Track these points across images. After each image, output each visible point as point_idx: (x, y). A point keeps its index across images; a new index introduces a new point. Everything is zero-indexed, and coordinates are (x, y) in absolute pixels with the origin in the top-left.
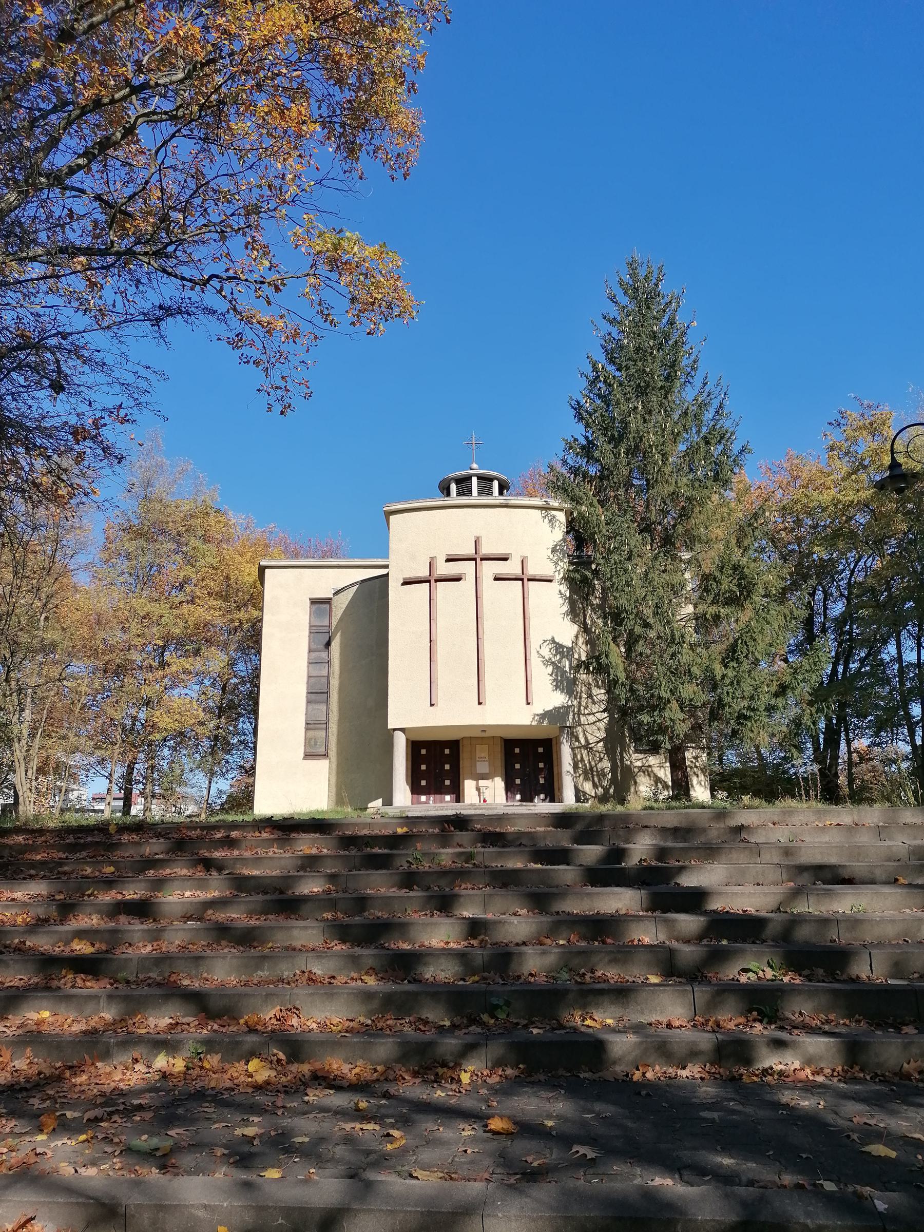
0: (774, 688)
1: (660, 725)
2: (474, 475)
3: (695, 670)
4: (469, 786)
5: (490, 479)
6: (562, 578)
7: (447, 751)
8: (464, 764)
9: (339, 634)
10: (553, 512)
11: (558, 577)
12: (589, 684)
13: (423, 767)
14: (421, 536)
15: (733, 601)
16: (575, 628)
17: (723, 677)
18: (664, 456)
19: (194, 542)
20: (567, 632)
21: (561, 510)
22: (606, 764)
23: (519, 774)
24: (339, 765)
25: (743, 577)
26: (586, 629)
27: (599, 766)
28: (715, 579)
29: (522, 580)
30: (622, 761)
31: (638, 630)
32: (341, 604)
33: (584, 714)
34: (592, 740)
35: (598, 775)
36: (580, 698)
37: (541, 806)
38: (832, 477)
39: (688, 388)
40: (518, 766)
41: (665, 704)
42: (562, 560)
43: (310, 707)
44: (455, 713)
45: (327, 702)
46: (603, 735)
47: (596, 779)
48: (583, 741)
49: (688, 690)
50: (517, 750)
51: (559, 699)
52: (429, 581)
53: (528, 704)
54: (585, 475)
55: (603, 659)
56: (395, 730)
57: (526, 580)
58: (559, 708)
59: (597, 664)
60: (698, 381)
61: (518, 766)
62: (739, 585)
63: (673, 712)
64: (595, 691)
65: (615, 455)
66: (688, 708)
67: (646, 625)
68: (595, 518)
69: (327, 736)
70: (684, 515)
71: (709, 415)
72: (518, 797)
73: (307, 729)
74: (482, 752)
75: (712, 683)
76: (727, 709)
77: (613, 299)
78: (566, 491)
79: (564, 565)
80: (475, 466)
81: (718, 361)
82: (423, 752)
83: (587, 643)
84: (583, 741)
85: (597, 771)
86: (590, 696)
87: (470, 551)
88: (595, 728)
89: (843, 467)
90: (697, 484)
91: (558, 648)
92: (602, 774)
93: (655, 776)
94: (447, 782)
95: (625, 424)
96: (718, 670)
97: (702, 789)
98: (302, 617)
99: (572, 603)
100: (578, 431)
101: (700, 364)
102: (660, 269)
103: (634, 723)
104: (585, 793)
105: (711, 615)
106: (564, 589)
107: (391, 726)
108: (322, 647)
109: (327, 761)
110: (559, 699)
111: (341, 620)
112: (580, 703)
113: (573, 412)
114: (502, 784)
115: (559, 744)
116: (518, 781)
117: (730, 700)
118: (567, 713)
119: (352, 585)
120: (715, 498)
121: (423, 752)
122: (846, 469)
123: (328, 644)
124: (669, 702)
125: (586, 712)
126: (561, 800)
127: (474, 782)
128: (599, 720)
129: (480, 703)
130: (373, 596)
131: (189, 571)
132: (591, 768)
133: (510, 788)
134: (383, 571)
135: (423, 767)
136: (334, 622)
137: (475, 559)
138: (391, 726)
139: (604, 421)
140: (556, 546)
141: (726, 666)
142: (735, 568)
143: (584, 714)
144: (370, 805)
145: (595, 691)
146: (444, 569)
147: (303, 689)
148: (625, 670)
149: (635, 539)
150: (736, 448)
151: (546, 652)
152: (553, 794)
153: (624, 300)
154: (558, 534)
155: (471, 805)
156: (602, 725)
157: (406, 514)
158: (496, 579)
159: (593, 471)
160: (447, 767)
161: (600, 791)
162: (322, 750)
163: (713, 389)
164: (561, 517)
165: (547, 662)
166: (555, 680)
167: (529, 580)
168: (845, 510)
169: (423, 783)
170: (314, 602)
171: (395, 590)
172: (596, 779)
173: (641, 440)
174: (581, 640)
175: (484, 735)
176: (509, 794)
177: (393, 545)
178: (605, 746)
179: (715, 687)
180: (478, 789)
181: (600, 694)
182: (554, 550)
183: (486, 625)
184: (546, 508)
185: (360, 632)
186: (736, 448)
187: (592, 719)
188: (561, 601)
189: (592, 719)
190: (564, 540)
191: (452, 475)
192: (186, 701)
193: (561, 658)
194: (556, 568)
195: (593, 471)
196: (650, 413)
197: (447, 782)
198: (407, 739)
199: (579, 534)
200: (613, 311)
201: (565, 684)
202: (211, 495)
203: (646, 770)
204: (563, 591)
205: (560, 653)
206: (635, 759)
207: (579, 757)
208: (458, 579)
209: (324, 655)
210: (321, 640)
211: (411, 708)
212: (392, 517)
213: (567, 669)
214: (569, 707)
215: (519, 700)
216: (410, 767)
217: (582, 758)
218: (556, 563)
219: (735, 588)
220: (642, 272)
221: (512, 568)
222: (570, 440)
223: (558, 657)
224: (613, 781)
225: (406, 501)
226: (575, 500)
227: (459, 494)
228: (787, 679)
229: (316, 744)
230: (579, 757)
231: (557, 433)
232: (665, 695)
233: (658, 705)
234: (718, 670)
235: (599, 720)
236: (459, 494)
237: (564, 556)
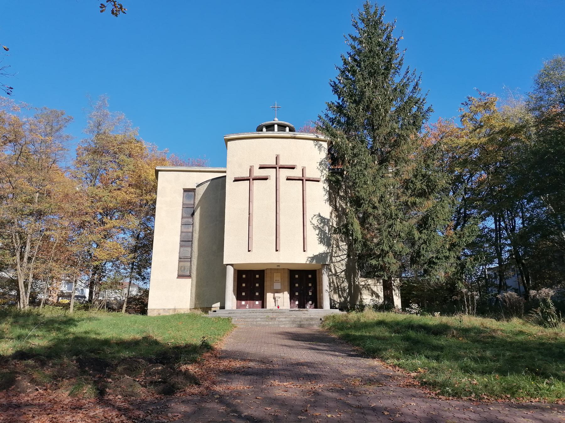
2: (276, 124)
3: (403, 235)
4: (269, 296)
6: (325, 180)
7: (257, 276)
8: (267, 284)
9: (199, 208)
10: (321, 142)
11: (323, 179)
12: (338, 240)
13: (244, 285)
14: (244, 154)
15: (423, 194)
17: (419, 238)
18: (386, 111)
19: (122, 157)
20: (326, 211)
21: (326, 141)
22: (346, 284)
23: (298, 290)
24: (197, 282)
25: (429, 180)
26: (336, 209)
27: (342, 285)
28: (412, 182)
29: (302, 180)
30: (354, 282)
31: (370, 210)
32: (201, 191)
33: (334, 257)
34: (338, 271)
35: (341, 290)
36: (333, 247)
37: (310, 312)
38: (464, 131)
39: (397, 76)
40: (297, 285)
41: (385, 254)
42: (325, 170)
43: (182, 249)
44: (262, 256)
46: (344, 268)
47: (340, 293)
48: (333, 271)
49: (399, 246)
50: (297, 276)
51: (322, 249)
52: (249, 180)
53: (304, 251)
54: (339, 122)
55: (350, 227)
56: (227, 265)
57: (304, 180)
58: (322, 254)
59: (344, 230)
60: (403, 71)
61: (297, 285)
62: (427, 186)
64: (341, 243)
65: (356, 111)
66: (398, 255)
67: (375, 208)
68: (344, 146)
69: (191, 265)
70: (396, 144)
71: (408, 91)
72: (297, 303)
73: (179, 261)
74: (277, 277)
75: (412, 242)
76: (422, 258)
77: (356, 26)
78: (328, 131)
79: (326, 172)
80: (276, 119)
81: (413, 61)
82: (244, 276)
83: (337, 217)
84: (333, 271)
85: (341, 288)
86: (338, 246)
87: (273, 163)
88: (340, 264)
89: (470, 126)
90: (404, 127)
91: (323, 220)
92: (343, 290)
93: (372, 290)
94: (257, 294)
95: (363, 93)
96: (417, 234)
97: (397, 298)
98: (179, 199)
100: (335, 99)
101: (404, 62)
102: (382, 8)
103: (363, 261)
104: (334, 301)
105: (411, 202)
106: (326, 186)
108: (190, 215)
109: (190, 280)
110: (322, 249)
111: (200, 201)
112: (332, 250)
113: (332, 88)
114: (288, 296)
115: (322, 274)
116: (297, 294)
117: (424, 252)
118: (327, 257)
119: (207, 181)
120: (412, 136)
121: (244, 276)
122: (471, 127)
123: (193, 214)
124: (388, 252)
125: (336, 255)
126: (321, 307)
127: (272, 294)
128: (342, 260)
129: (277, 251)
130: (218, 187)
131: (120, 173)
132: (338, 287)
133: (292, 298)
135: (244, 285)
136: (197, 202)
137: (276, 168)
139: (350, 91)
140: (322, 161)
141: (421, 232)
142: (424, 176)
143: (334, 257)
144: (213, 306)
145: (341, 243)
146: (258, 173)
147: (178, 239)
149: (368, 158)
150: (425, 108)
151: (315, 222)
152: (318, 305)
153: (361, 26)
155: (271, 310)
156: (344, 262)
157: (237, 141)
158: (288, 179)
159: (343, 120)
160: (257, 285)
161: (343, 299)
162: (188, 273)
163: (411, 76)
164: (325, 145)
165: (316, 228)
166: (320, 238)
167: (306, 180)
168: (471, 147)
169: (244, 294)
170: (186, 190)
171: (230, 185)
172: (340, 293)
173: (371, 102)
174: (333, 215)
175: (278, 268)
176: (292, 301)
177: (229, 159)
178: (345, 274)
179: (413, 244)
180: (274, 298)
181: (344, 246)
182: (321, 164)
183: (282, 205)
184: (317, 140)
185: (209, 208)
186: (425, 108)
187: (338, 259)
188: (324, 193)
189: (338, 259)
190: (326, 158)
191: (264, 123)
192: (123, 240)
193: (324, 225)
194: (322, 174)
195: (343, 120)
196: (376, 88)
197: (257, 294)
198: (235, 270)
199: (335, 157)
200: (356, 33)
201: (325, 239)
202: (133, 132)
203: (367, 287)
204: (325, 187)
205: (323, 222)
206: (361, 281)
207: (331, 280)
208: (266, 179)
209: (190, 220)
210: (189, 212)
211: (236, 253)
212: (228, 143)
213: (327, 231)
214: (327, 253)
215: (299, 249)
216: (236, 277)
217: (333, 281)
218: (322, 171)
219: (425, 187)
220: (372, 11)
221: (297, 173)
223: (322, 224)
224: (350, 294)
225: (237, 133)
226: (334, 135)
228: (455, 240)
229: (184, 269)
230: (331, 280)
231: (322, 100)
232: (386, 248)
233: (384, 254)
234: (417, 234)
235: (342, 260)
237: (326, 167)
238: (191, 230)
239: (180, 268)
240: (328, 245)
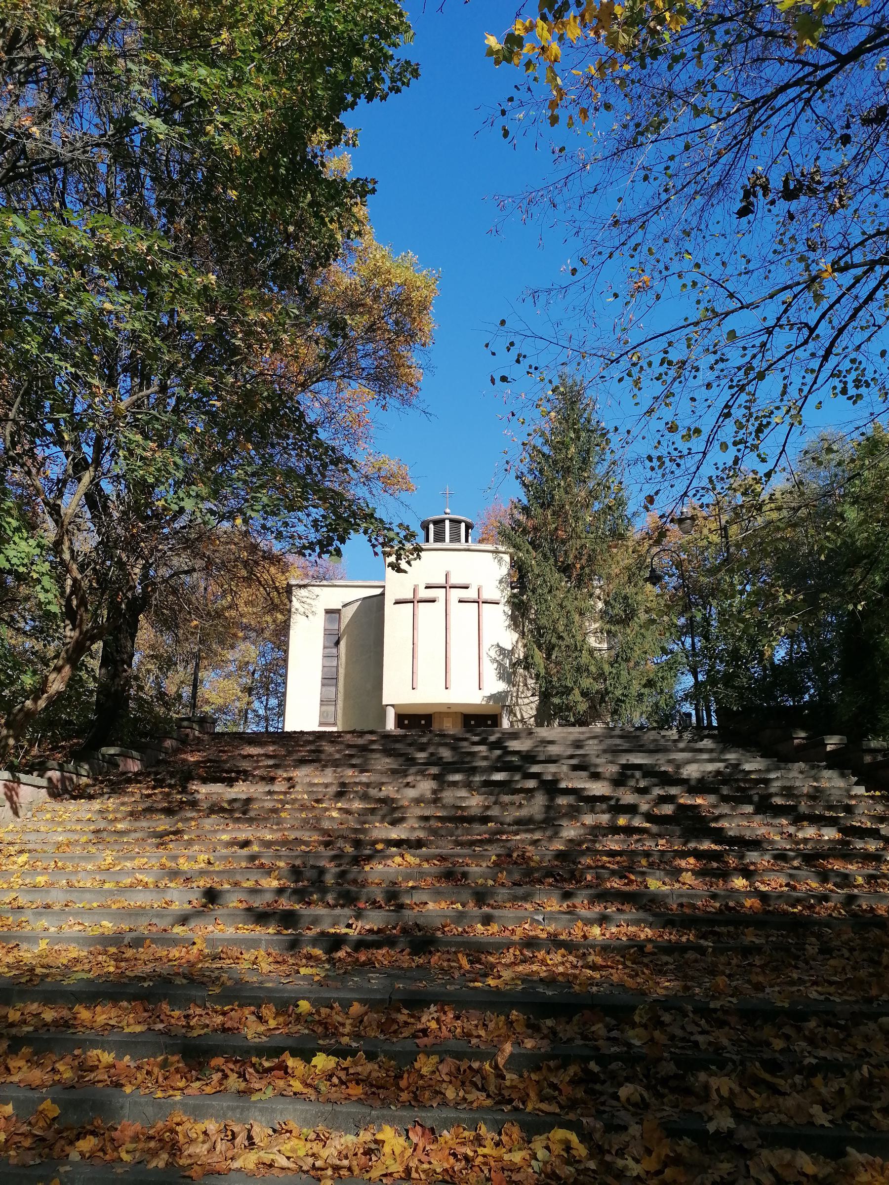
0: (644, 682)
1: (567, 705)
5: (459, 522)
7: (423, 722)
11: (504, 601)
16: (516, 636)
20: (509, 639)
31: (554, 640)
32: (348, 614)
34: (526, 716)
45: (336, 685)
49: (586, 682)
63: (576, 695)
67: (560, 638)
69: (336, 711)
79: (508, 592)
86: (526, 685)
87: (442, 581)
91: (502, 650)
99: (513, 618)
107: (384, 703)
111: (348, 625)
115: (501, 717)
123: (337, 643)
130: (372, 611)
134: (378, 591)
138: (384, 703)
142: (626, 598)
148: (546, 668)
151: (493, 653)
154: (504, 570)
156: (534, 706)
162: (332, 721)
164: (507, 558)
170: (328, 612)
171: (390, 609)
174: (520, 644)
178: (536, 721)
182: (501, 582)
184: (496, 552)
187: (526, 701)
189: (526, 701)
190: (509, 574)
199: (520, 577)
201: (506, 675)
209: (334, 651)
210: (333, 640)
221: (471, 594)
222: (516, 500)
227: (436, 541)
233: (568, 691)
236: (436, 541)
238: (335, 664)
239: (322, 714)
240: (509, 682)
